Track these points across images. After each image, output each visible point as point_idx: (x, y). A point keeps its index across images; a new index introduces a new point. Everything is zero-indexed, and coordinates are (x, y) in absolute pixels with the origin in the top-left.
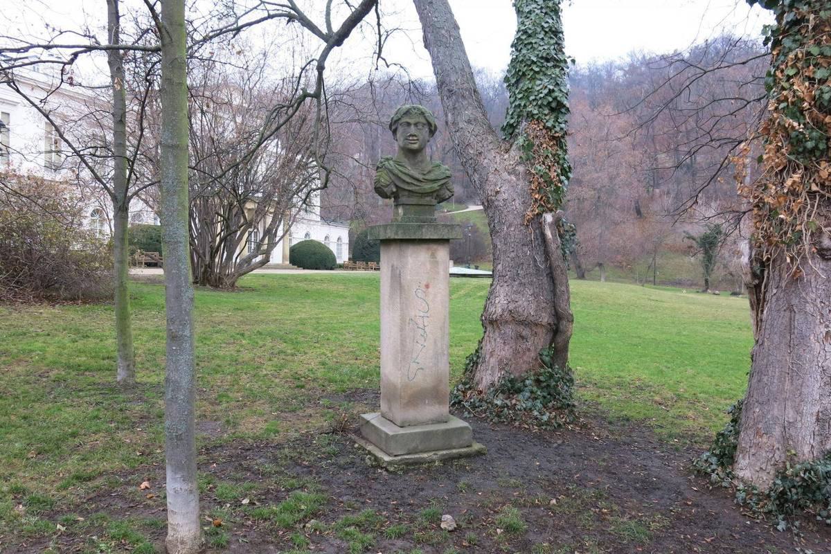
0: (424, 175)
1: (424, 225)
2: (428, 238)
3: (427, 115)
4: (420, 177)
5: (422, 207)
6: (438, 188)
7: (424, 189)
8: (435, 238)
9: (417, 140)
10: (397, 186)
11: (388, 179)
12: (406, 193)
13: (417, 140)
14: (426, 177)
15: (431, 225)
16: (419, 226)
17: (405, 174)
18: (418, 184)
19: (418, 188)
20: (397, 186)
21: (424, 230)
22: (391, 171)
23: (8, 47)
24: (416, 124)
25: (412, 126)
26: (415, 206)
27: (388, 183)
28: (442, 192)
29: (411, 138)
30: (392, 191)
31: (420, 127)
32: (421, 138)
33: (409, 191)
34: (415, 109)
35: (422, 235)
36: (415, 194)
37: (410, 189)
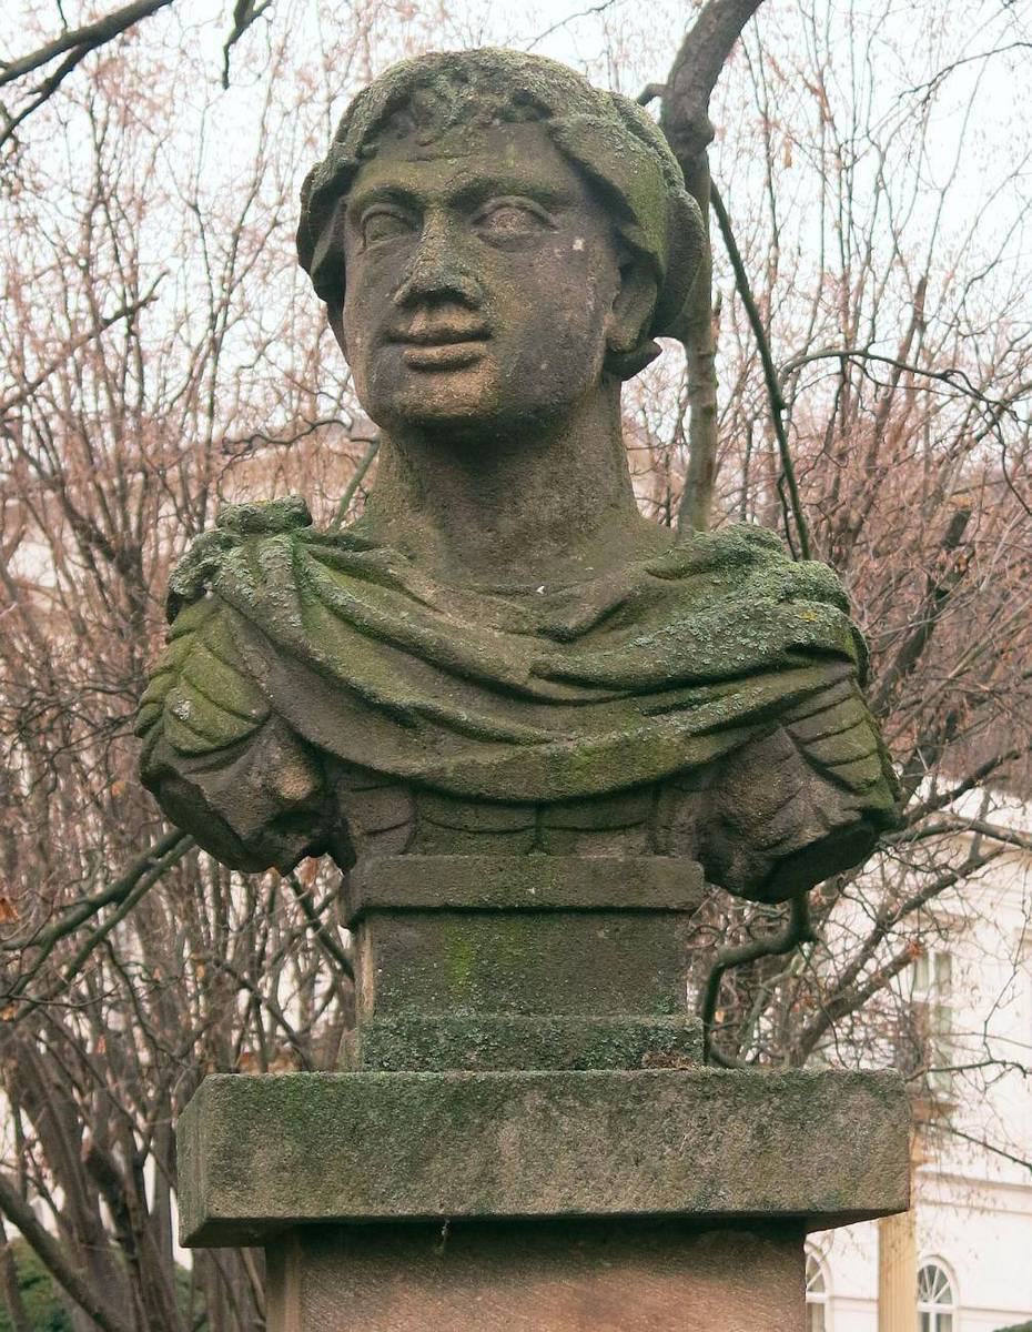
0: (564, 638)
1: (512, 1092)
2: (548, 1203)
3: (570, 119)
4: (515, 657)
5: (555, 933)
6: (700, 752)
7: (557, 762)
8: (619, 1206)
9: (481, 335)
10: (315, 757)
11: (237, 696)
12: (393, 809)
13: (481, 335)
14: (593, 660)
15: (583, 1094)
16: (459, 1098)
17: (381, 637)
18: (500, 720)
19: (501, 754)
20: (315, 757)
21: (508, 1135)
22: (255, 623)
23: (390, 899)
24: (468, 204)
25: (435, 225)
26: (481, 925)
27: (229, 727)
28: (758, 791)
29: (419, 324)
30: (271, 792)
31: (508, 223)
32: (511, 314)
33: (418, 788)
34: (460, 78)
35: (487, 1178)
36: (470, 817)
37: (416, 764)
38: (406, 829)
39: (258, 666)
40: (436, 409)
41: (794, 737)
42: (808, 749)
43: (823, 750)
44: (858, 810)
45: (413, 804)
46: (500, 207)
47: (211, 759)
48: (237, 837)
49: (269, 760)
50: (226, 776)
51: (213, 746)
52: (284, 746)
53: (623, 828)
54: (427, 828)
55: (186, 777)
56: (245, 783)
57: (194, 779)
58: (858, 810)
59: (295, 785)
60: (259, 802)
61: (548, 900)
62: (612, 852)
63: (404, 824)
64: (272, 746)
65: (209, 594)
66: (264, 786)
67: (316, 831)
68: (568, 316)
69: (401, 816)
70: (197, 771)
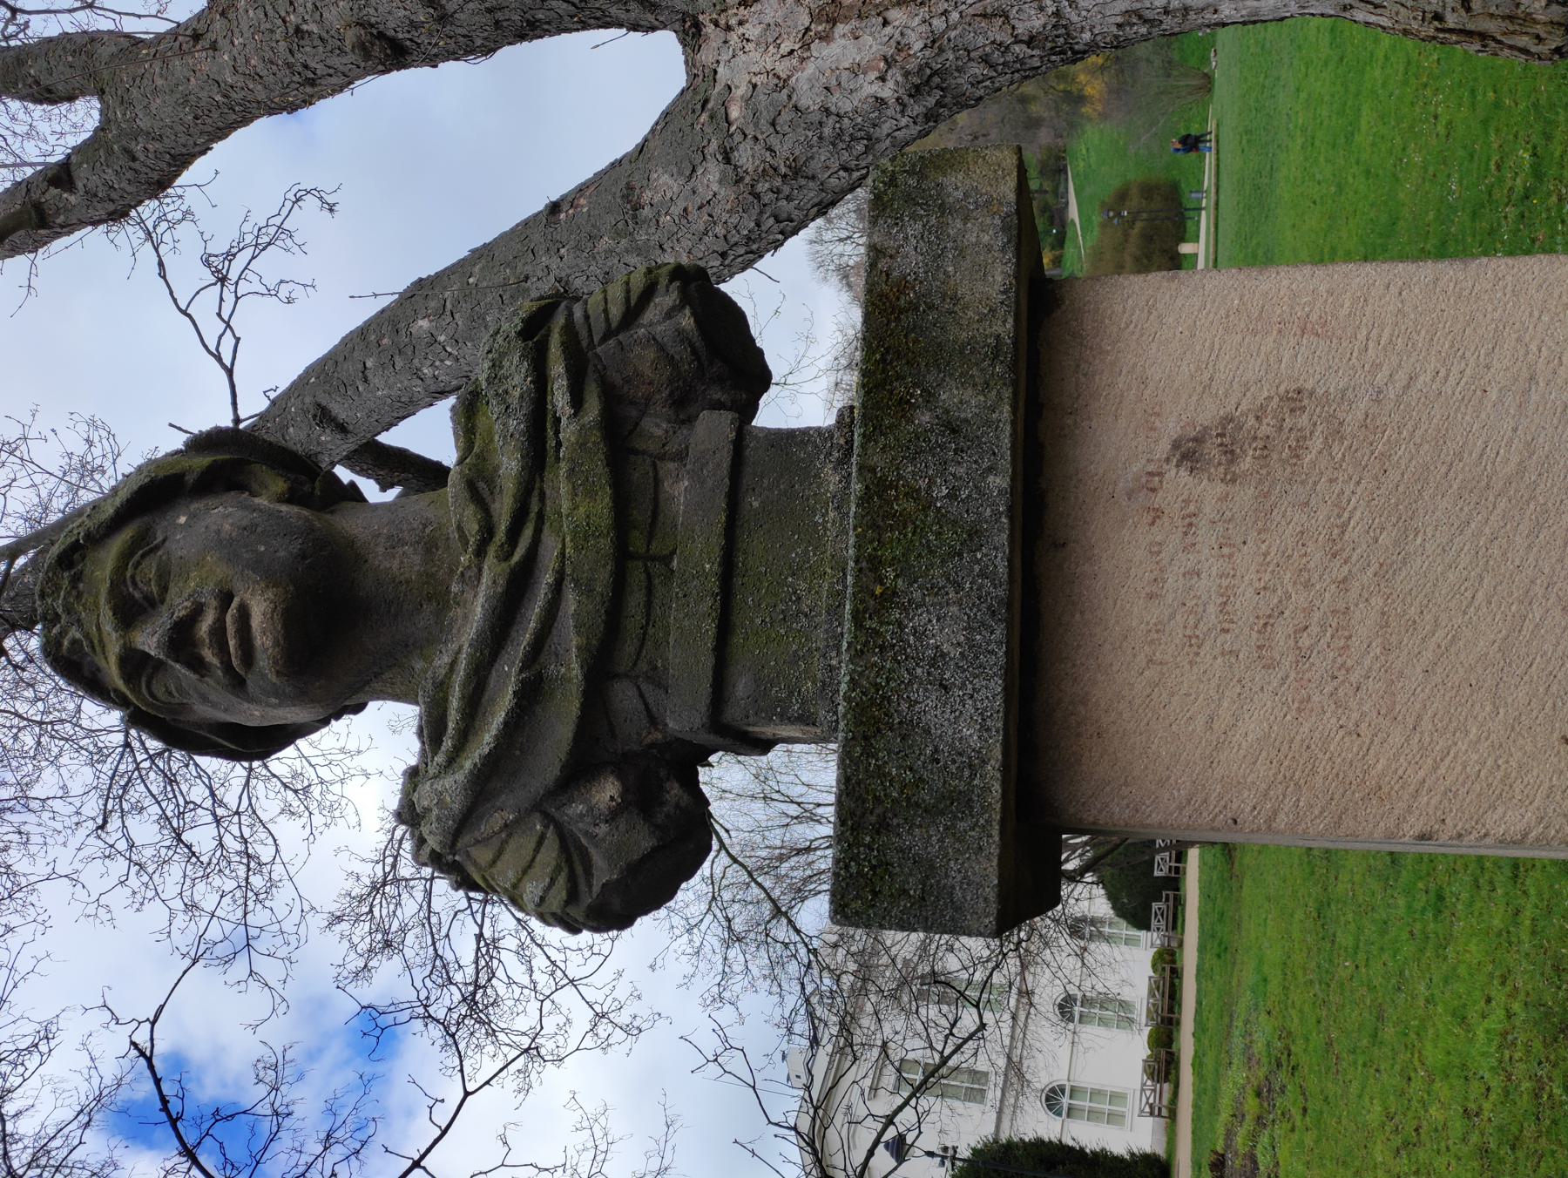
0: (488, 531)
4: (492, 574)
6: (593, 409)
11: (521, 846)
30: (613, 815)
38: (644, 687)
39: (496, 820)
40: (276, 643)
41: (604, 339)
42: (614, 325)
43: (616, 312)
44: (671, 282)
45: (617, 676)
46: (134, 584)
47: (579, 870)
48: (654, 850)
49: (582, 816)
50: (598, 859)
51: (566, 870)
52: (571, 800)
53: (657, 482)
54: (643, 666)
55: (594, 896)
56: (604, 840)
57: (596, 889)
58: (671, 282)
59: (607, 791)
60: (622, 827)
61: (717, 552)
62: (679, 490)
63: (639, 688)
64: (570, 812)
65: (457, 858)
66: (607, 822)
67: (663, 773)
68: (227, 527)
69: (632, 692)
70: (590, 886)
